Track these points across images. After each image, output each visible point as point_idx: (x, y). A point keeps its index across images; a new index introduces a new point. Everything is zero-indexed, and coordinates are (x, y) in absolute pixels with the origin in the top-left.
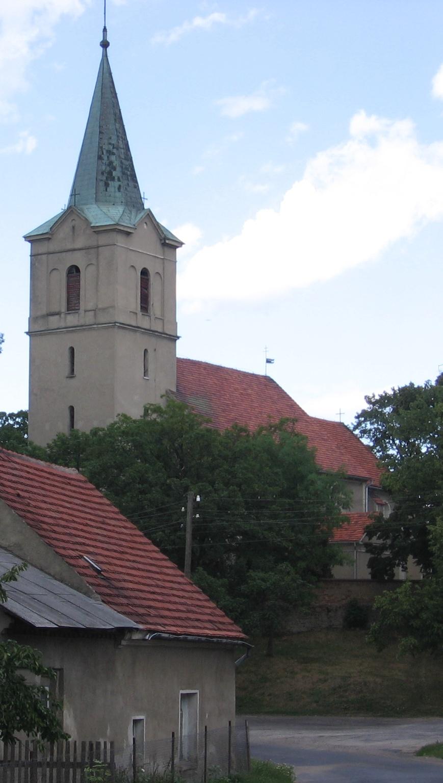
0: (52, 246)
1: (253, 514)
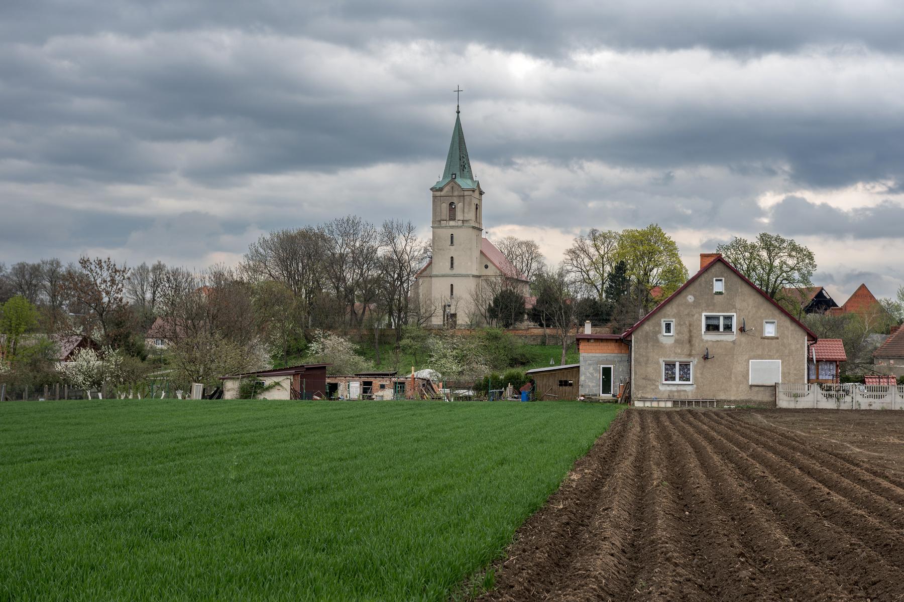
0: (442, 193)
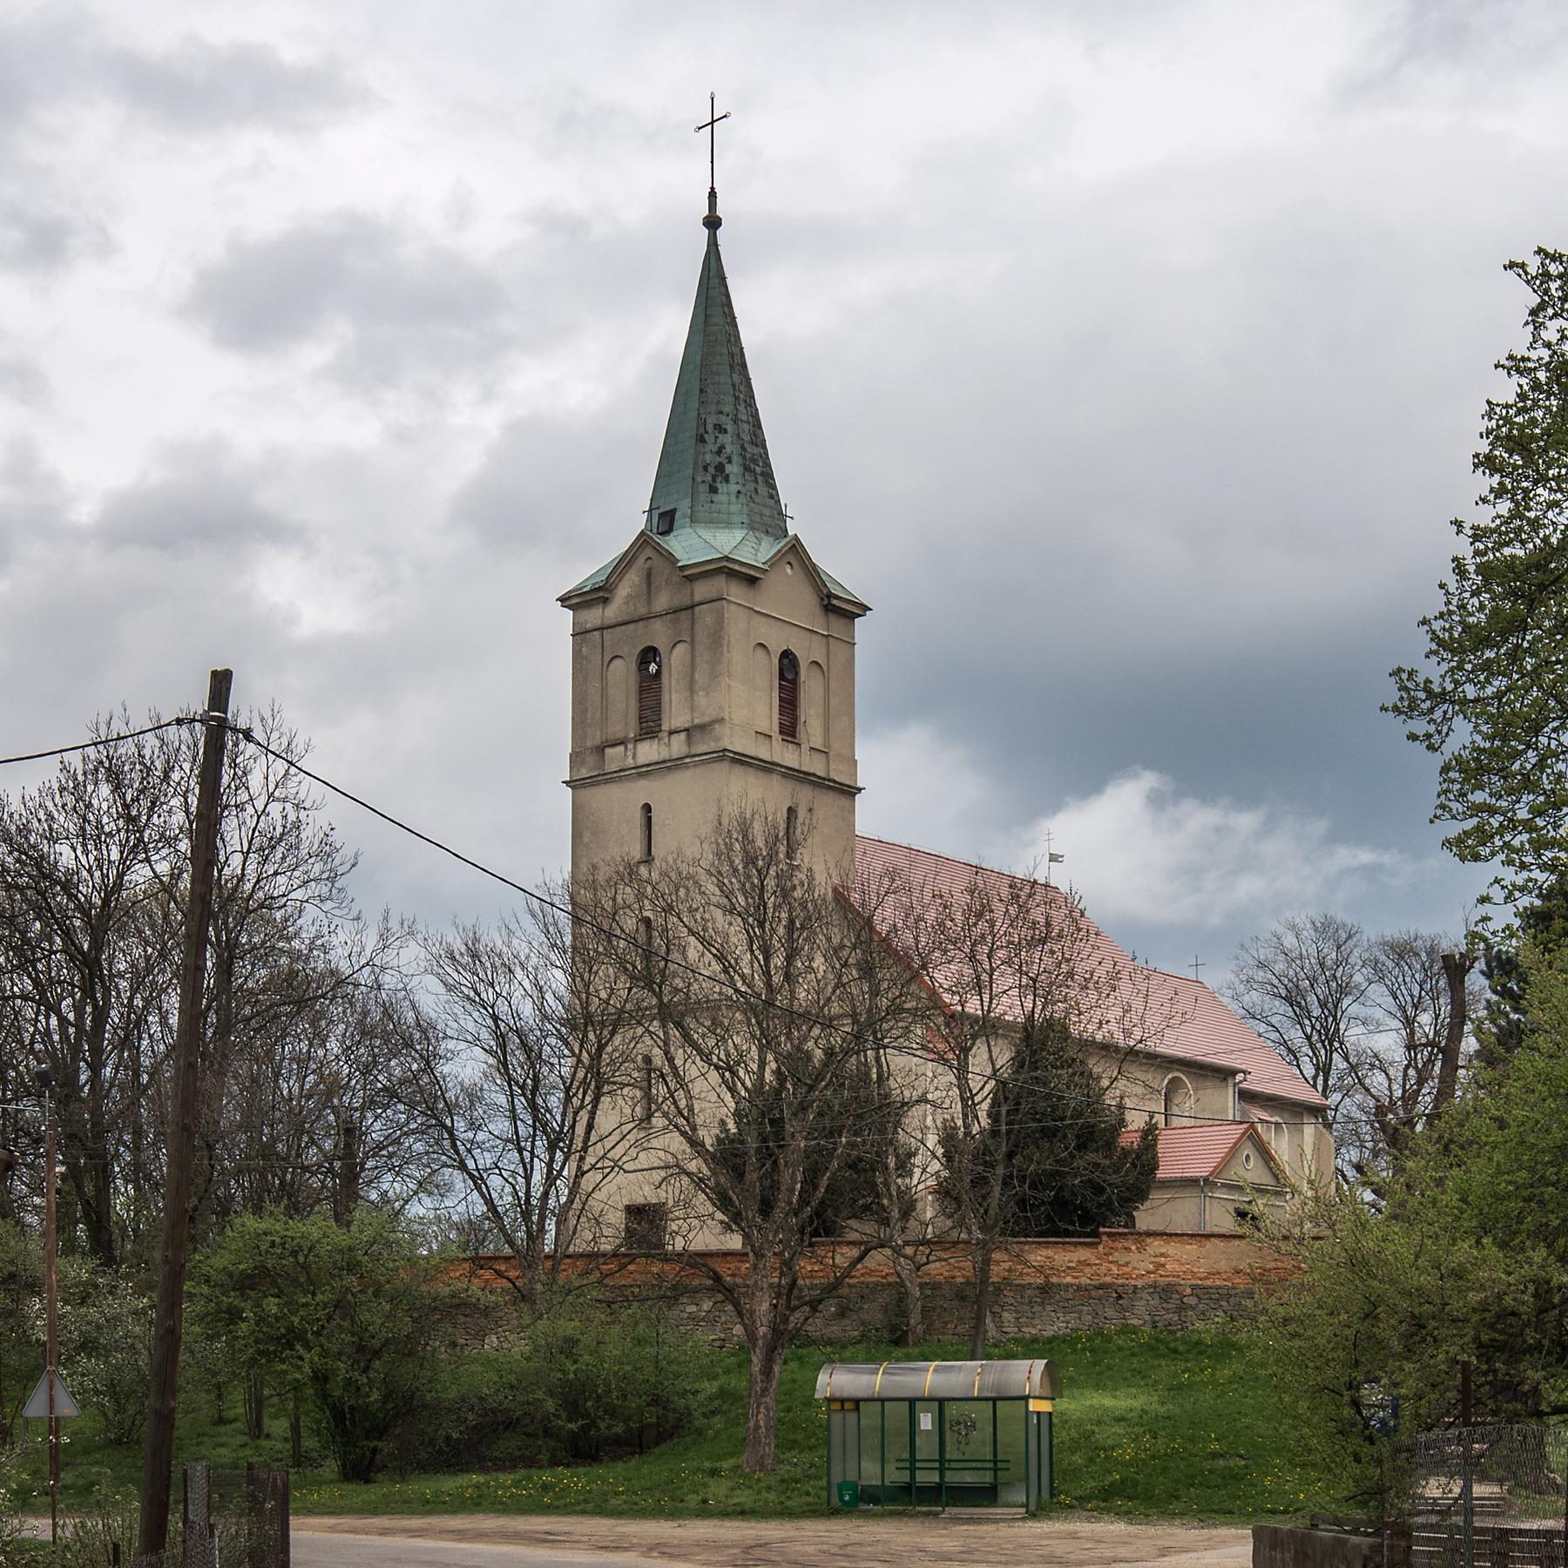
0: (612, 612)
1: (1120, 1349)
